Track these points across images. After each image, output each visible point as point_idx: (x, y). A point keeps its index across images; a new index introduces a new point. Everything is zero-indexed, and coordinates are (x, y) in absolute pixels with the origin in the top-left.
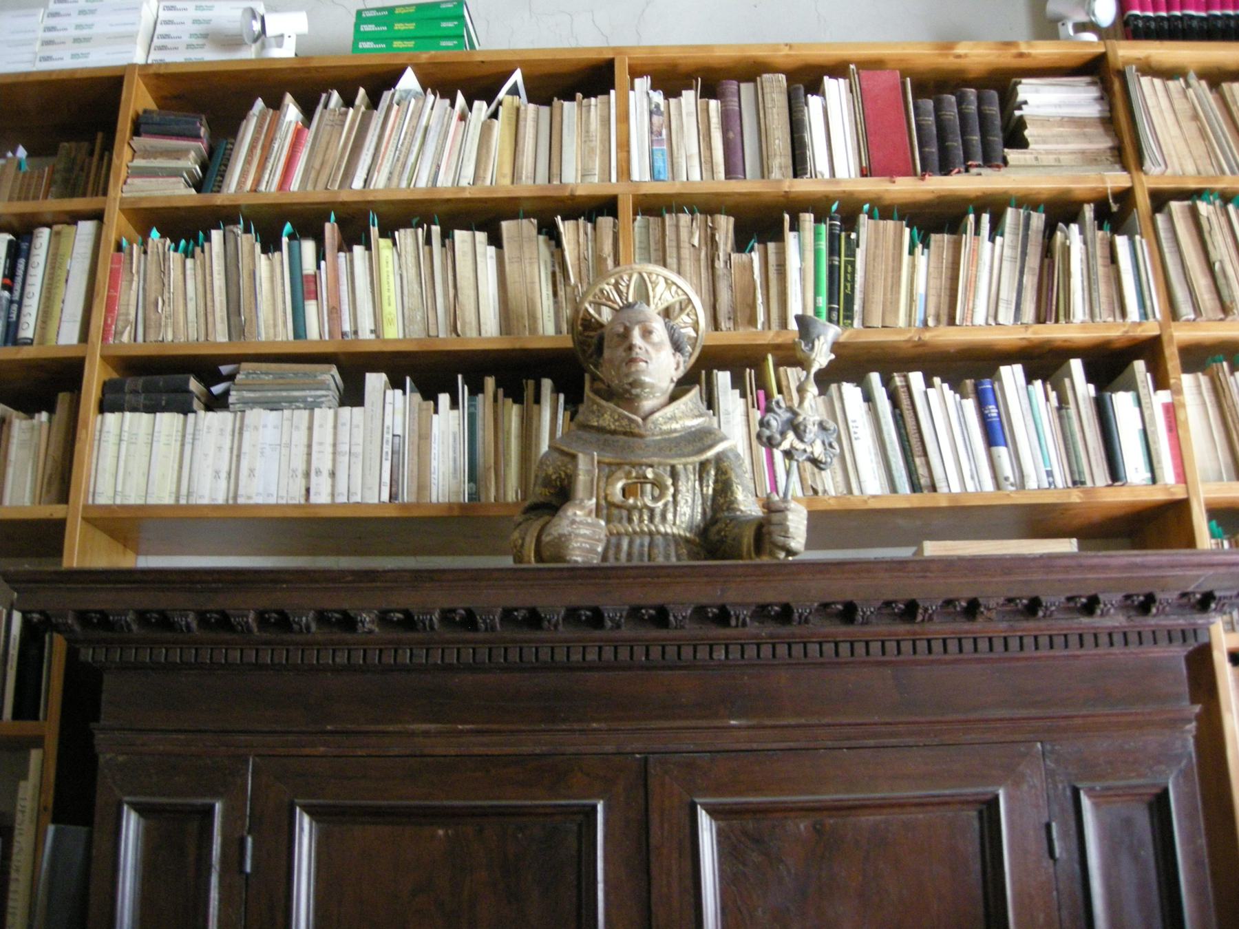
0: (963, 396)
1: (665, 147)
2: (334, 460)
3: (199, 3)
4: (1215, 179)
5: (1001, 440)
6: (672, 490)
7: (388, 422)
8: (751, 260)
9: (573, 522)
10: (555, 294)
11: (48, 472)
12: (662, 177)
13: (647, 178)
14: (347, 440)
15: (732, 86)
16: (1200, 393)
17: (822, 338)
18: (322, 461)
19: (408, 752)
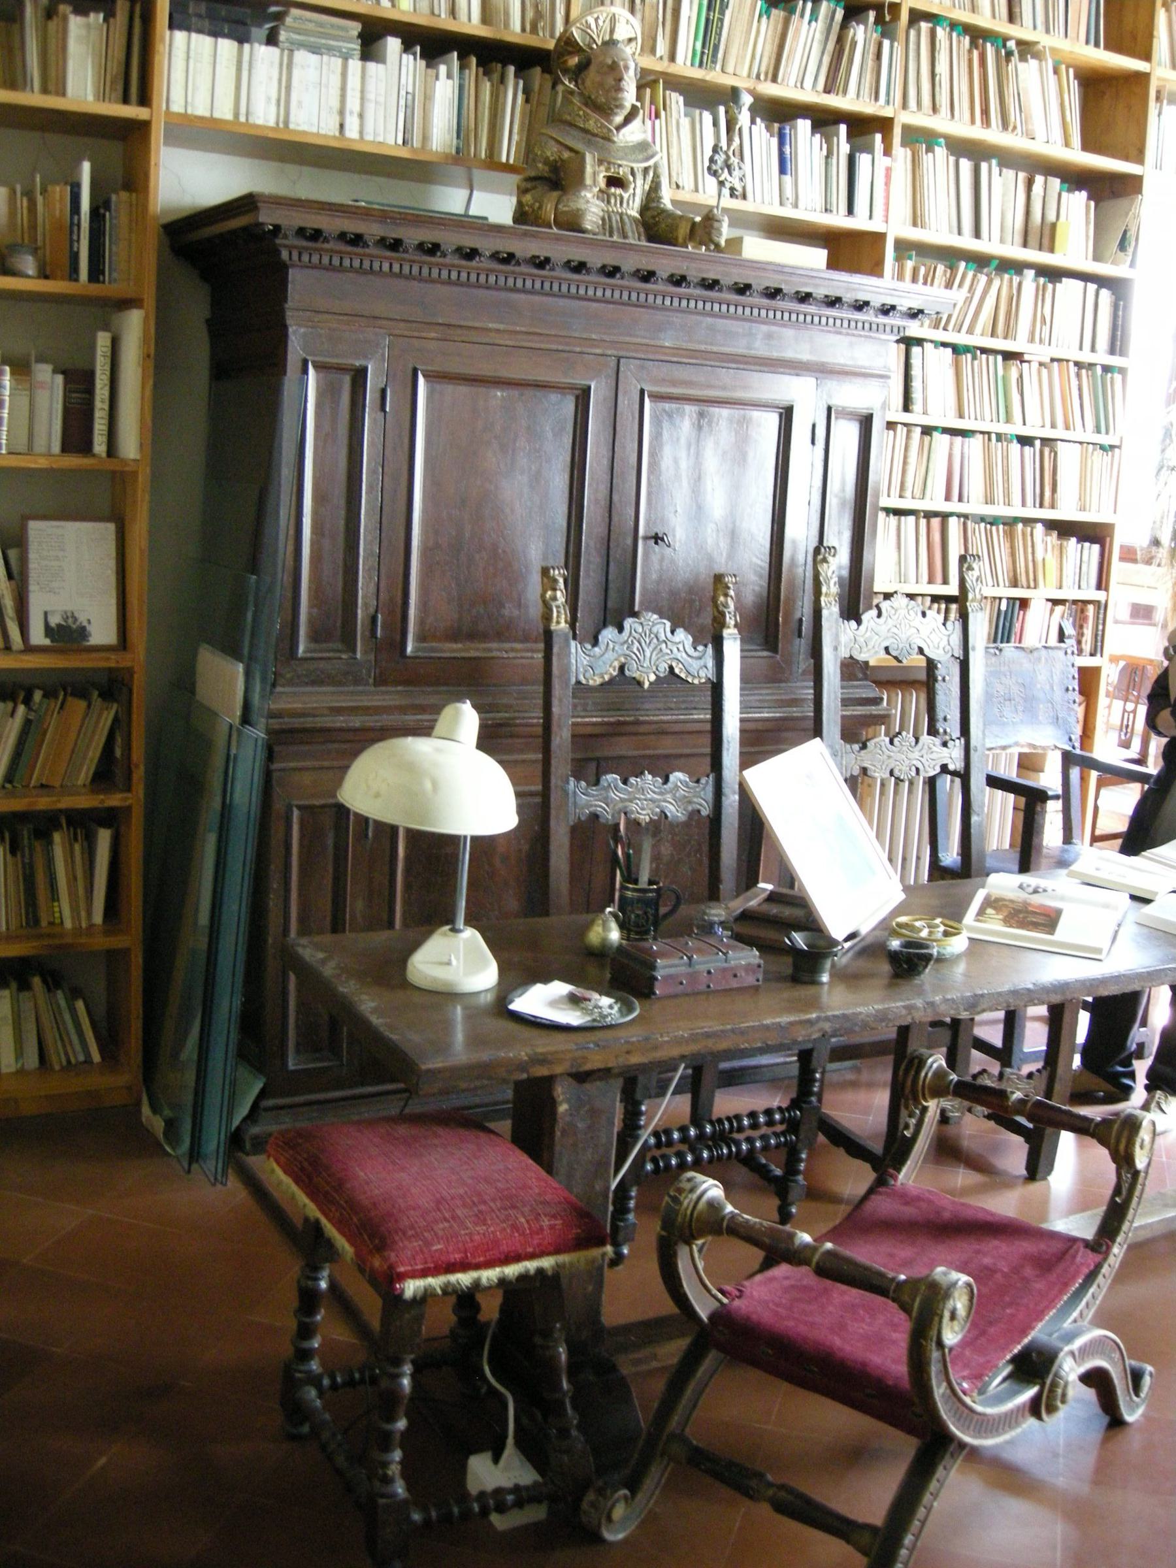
0: (772, 135)
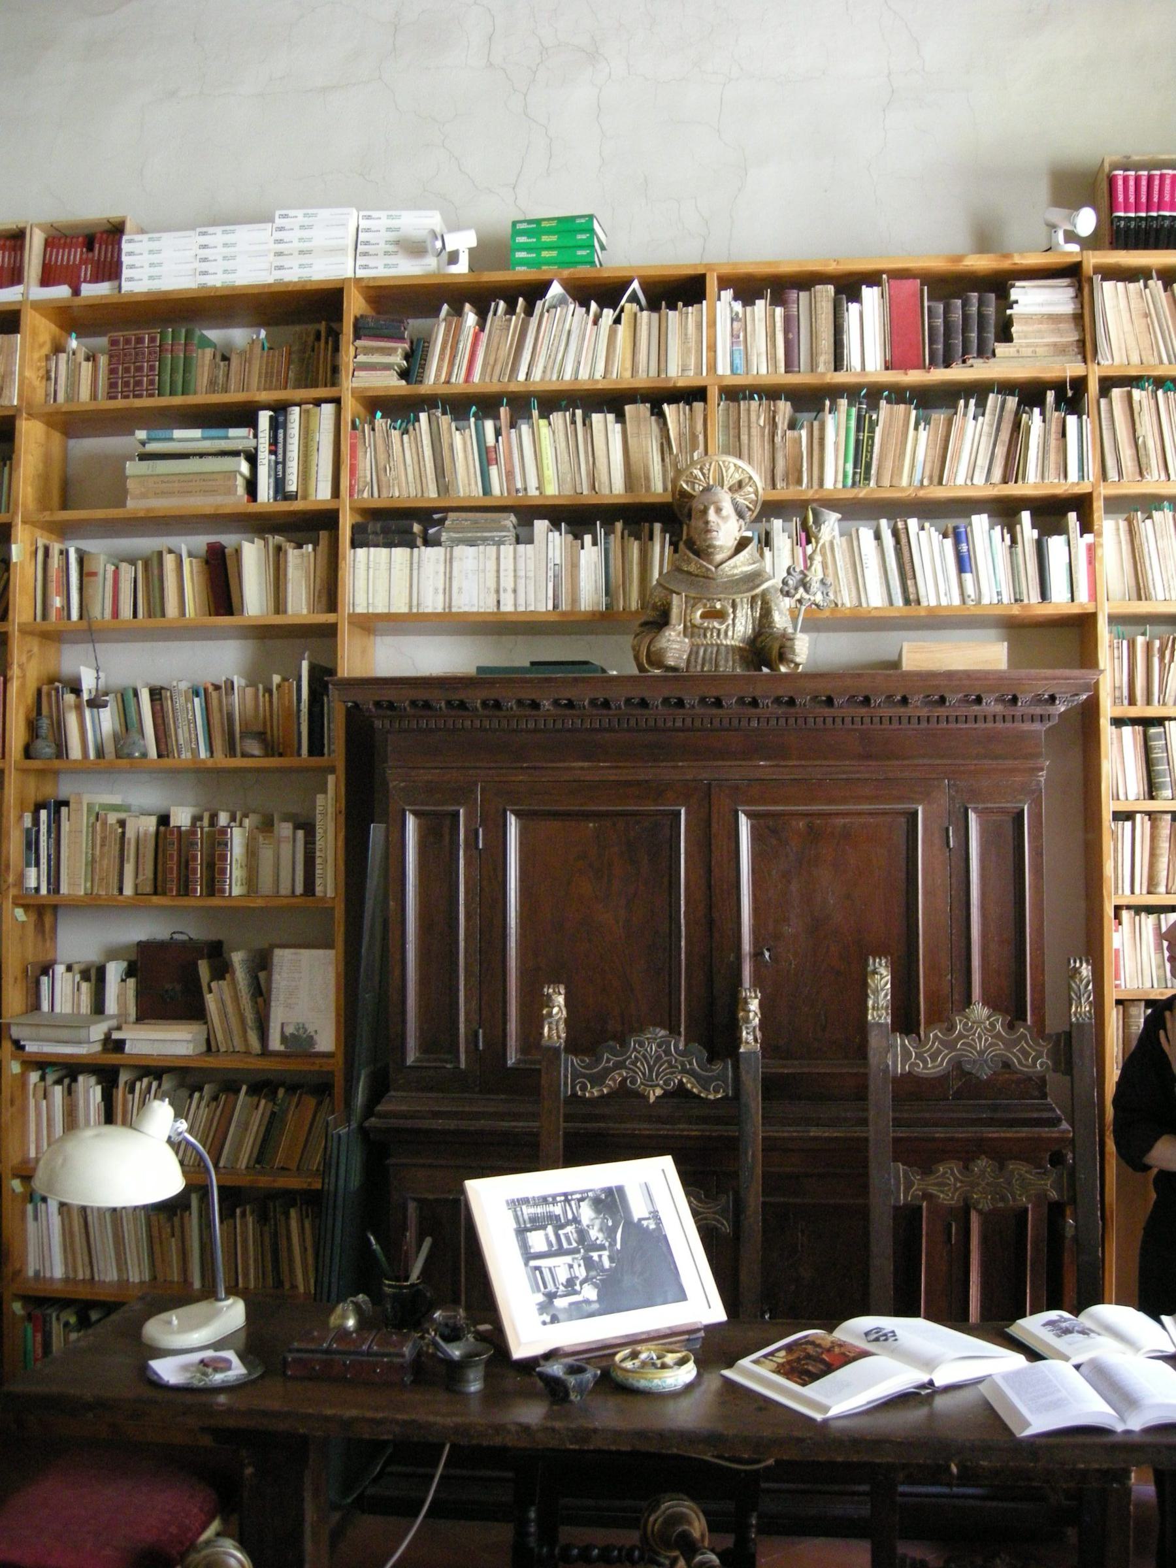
1: (742, 348)
2: (515, 582)
3: (390, 213)
4: (1154, 367)
5: (968, 568)
6: (732, 616)
7: (550, 555)
8: (800, 437)
9: (669, 640)
10: (663, 460)
11: (318, 587)
12: (739, 372)
13: (728, 372)
14: (523, 567)
15: (793, 294)
16: (1118, 535)
17: (826, 523)
18: (507, 582)
19: (572, 779)
